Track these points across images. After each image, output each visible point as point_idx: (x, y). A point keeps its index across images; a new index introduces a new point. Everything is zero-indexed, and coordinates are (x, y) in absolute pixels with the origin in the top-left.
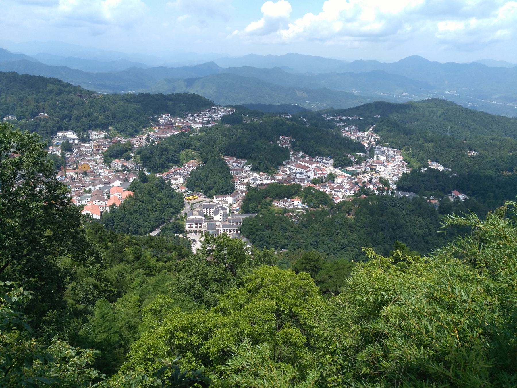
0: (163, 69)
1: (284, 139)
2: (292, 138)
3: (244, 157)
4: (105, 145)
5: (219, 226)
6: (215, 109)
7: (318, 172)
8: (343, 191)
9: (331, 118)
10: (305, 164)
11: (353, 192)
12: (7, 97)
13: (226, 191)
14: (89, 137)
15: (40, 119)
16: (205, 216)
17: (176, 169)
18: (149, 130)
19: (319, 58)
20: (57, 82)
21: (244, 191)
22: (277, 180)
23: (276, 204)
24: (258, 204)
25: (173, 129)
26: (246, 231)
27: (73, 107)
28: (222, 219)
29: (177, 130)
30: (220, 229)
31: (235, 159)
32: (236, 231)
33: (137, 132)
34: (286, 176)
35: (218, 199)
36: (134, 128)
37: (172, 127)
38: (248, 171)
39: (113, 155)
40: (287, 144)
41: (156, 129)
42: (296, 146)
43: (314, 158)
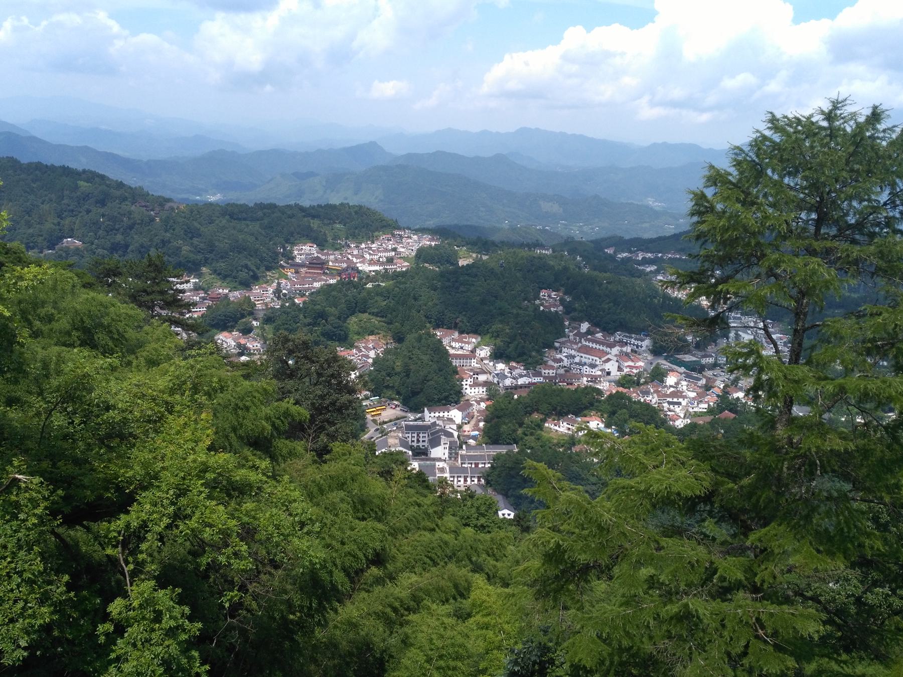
1: (549, 296)
2: (565, 294)
5: (442, 470)
6: (401, 236)
7: (626, 364)
8: (684, 403)
11: (706, 406)
13: (446, 398)
15: (67, 250)
18: (277, 276)
20: (97, 179)
21: (482, 400)
22: (545, 378)
23: (552, 426)
24: (517, 426)
25: (325, 273)
27: (131, 228)
28: (447, 455)
29: (332, 276)
30: (445, 475)
31: (456, 335)
32: (476, 480)
33: (255, 278)
35: (432, 414)
36: (249, 270)
37: (321, 269)
40: (555, 306)
43: (612, 334)
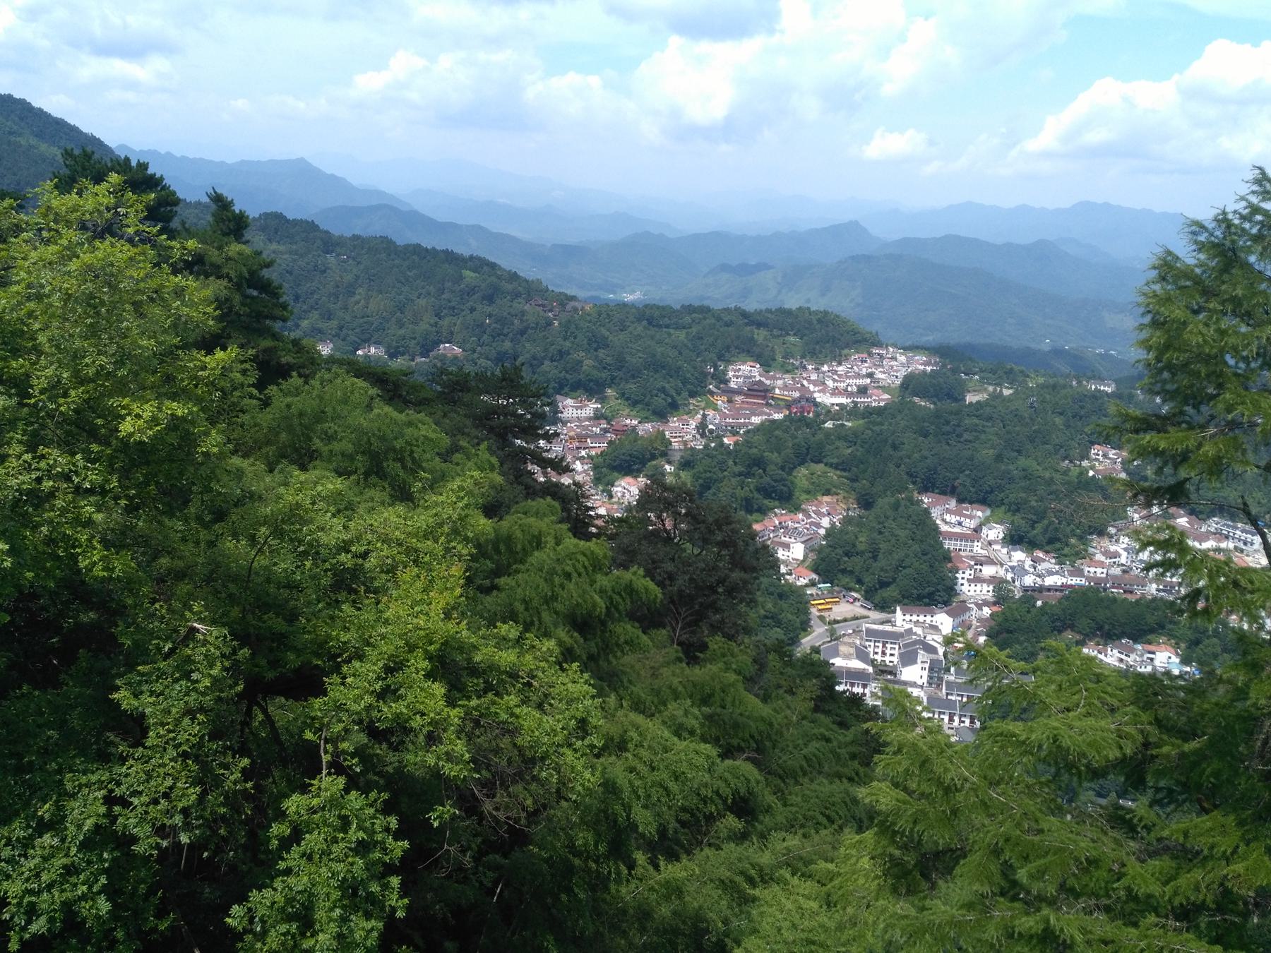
0: (718, 238)
1: (1105, 456)
3: (982, 500)
4: (595, 437)
6: (881, 356)
12: (368, 298)
14: (556, 412)
16: (872, 662)
17: (783, 518)
18: (703, 404)
21: (986, 603)
22: (1088, 579)
25: (768, 404)
27: (522, 333)
28: (925, 679)
29: (778, 408)
32: (967, 721)
33: (674, 407)
34: (1116, 571)
35: (908, 617)
36: (667, 395)
37: (764, 398)
38: (996, 542)
39: (620, 465)
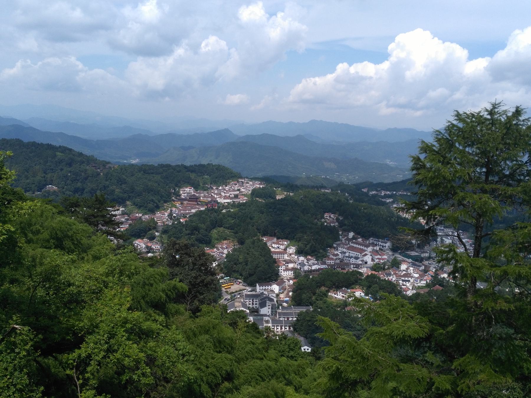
0: (172, 137)
1: (330, 217)
2: (339, 215)
6: (242, 182)
7: (376, 257)
9: (374, 192)
10: (361, 247)
11: (425, 282)
13: (269, 277)
15: (48, 192)
18: (170, 206)
19: (347, 126)
20: (67, 151)
21: (291, 279)
22: (328, 265)
23: (333, 295)
25: (198, 204)
26: (303, 328)
27: (86, 179)
28: (270, 313)
29: (202, 206)
33: (158, 208)
34: (338, 261)
35: (261, 288)
37: (196, 201)
38: (292, 254)
41: (178, 204)
42: (345, 225)
